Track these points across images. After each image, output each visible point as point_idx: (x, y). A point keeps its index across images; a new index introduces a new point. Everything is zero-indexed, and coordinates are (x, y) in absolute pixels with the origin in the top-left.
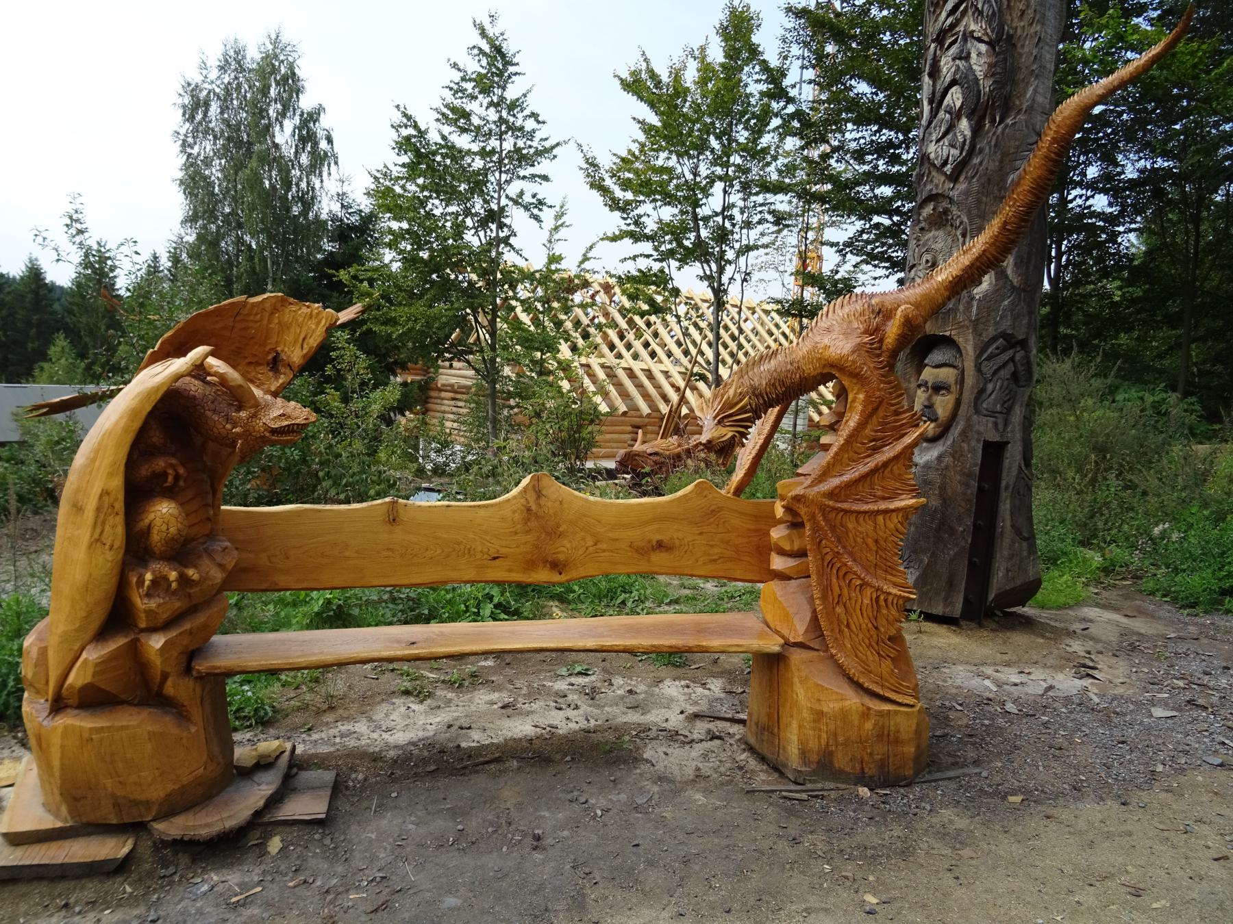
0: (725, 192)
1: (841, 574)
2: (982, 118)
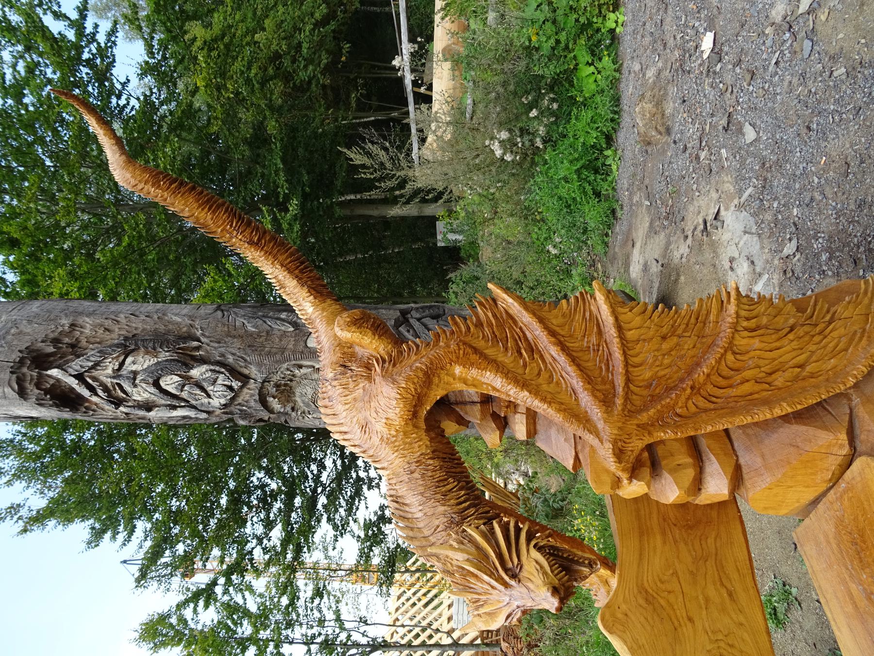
0: (291, 643)
1: (722, 382)
2: (193, 358)
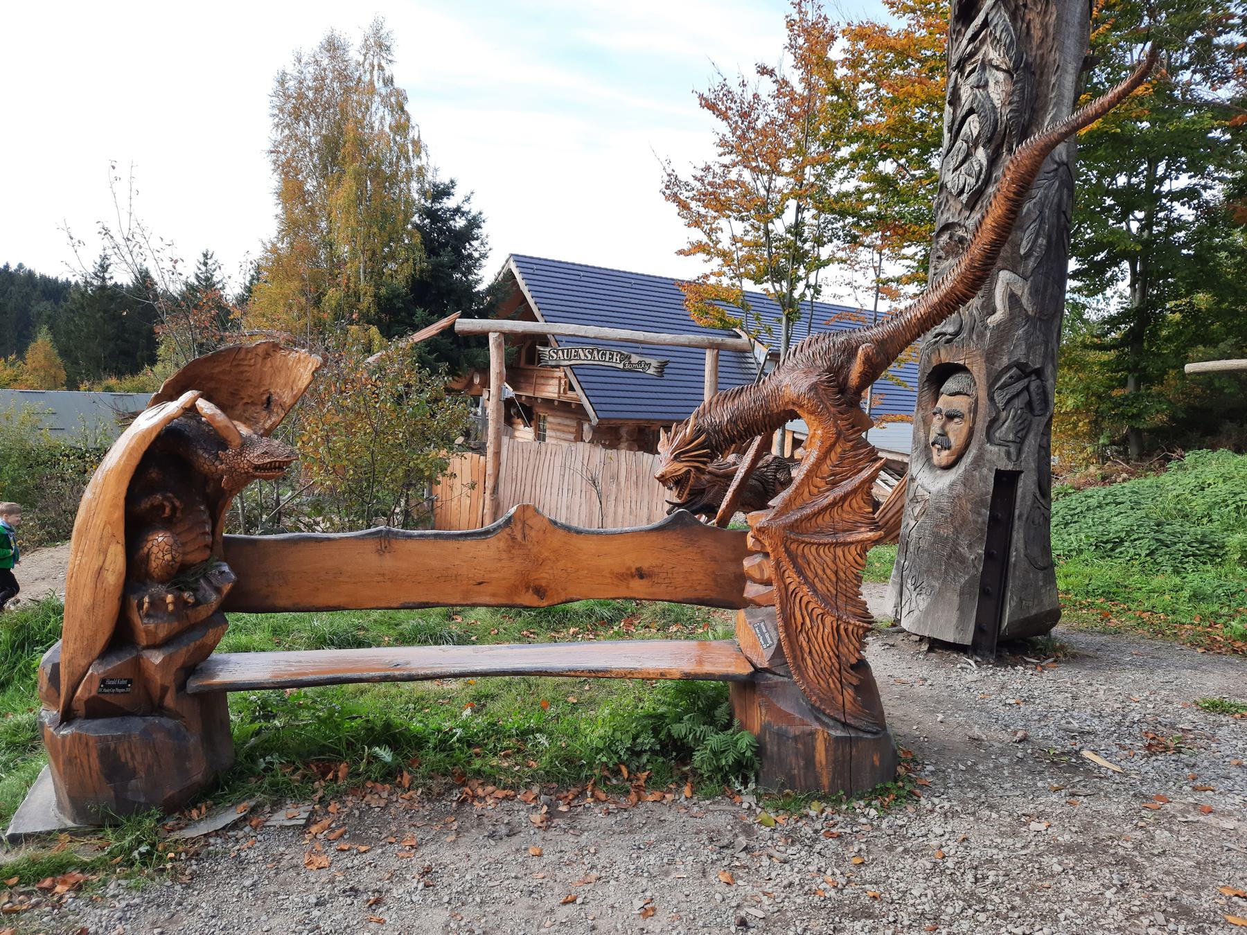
2: (1000, 146)
